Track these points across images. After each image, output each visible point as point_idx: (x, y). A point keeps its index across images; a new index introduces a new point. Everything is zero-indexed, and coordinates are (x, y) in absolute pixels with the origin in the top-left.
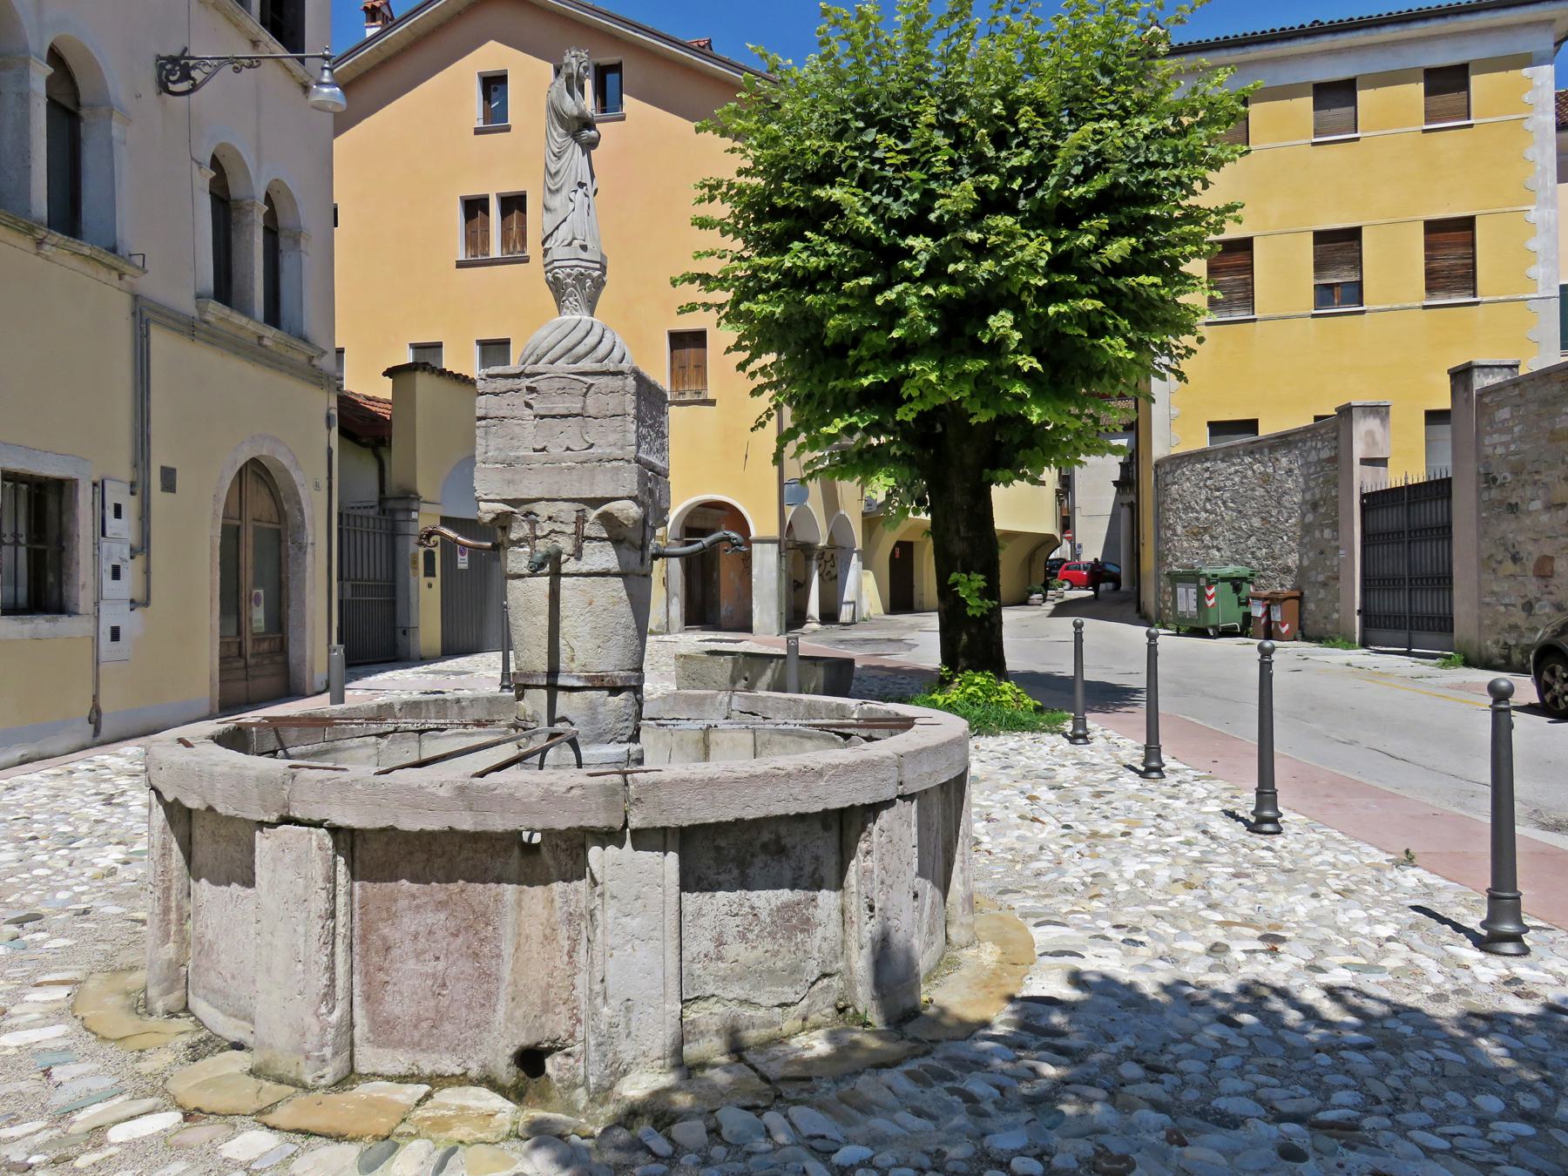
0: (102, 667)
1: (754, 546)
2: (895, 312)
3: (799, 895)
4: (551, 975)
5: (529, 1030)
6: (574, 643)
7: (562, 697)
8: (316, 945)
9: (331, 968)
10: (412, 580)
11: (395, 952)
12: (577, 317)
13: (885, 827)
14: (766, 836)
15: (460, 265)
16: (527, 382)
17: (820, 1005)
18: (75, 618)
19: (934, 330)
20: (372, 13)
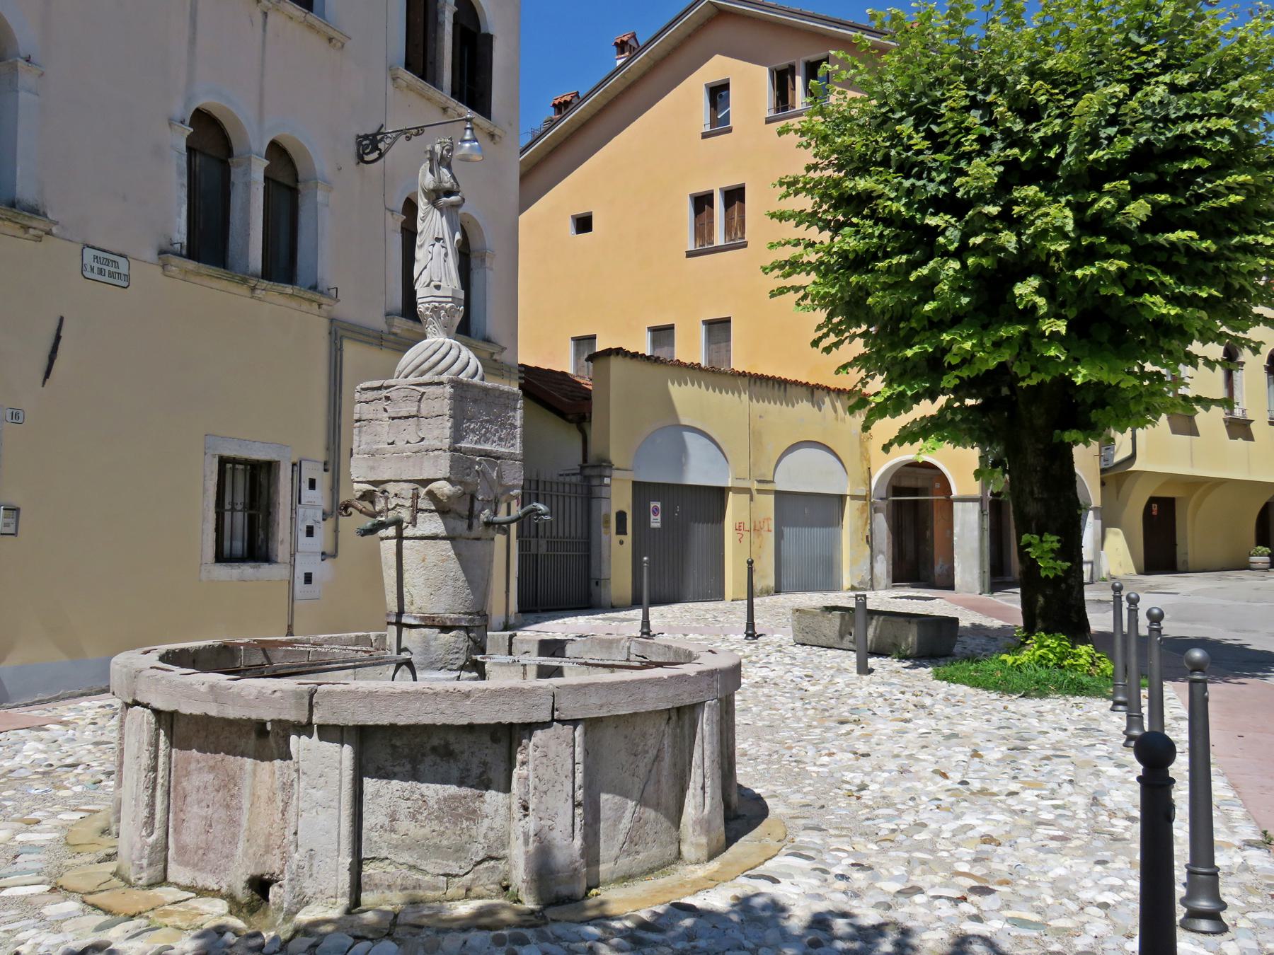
0: (296, 603)
1: (955, 504)
2: (927, 287)
3: (465, 791)
4: (271, 826)
5: (257, 864)
6: (413, 590)
7: (405, 631)
8: (142, 787)
9: (151, 805)
10: (604, 538)
11: (189, 799)
12: (441, 340)
13: (540, 743)
14: (436, 741)
15: (690, 254)
16: (384, 393)
17: (484, 880)
18: (274, 566)
19: (965, 300)
20: (621, 47)
